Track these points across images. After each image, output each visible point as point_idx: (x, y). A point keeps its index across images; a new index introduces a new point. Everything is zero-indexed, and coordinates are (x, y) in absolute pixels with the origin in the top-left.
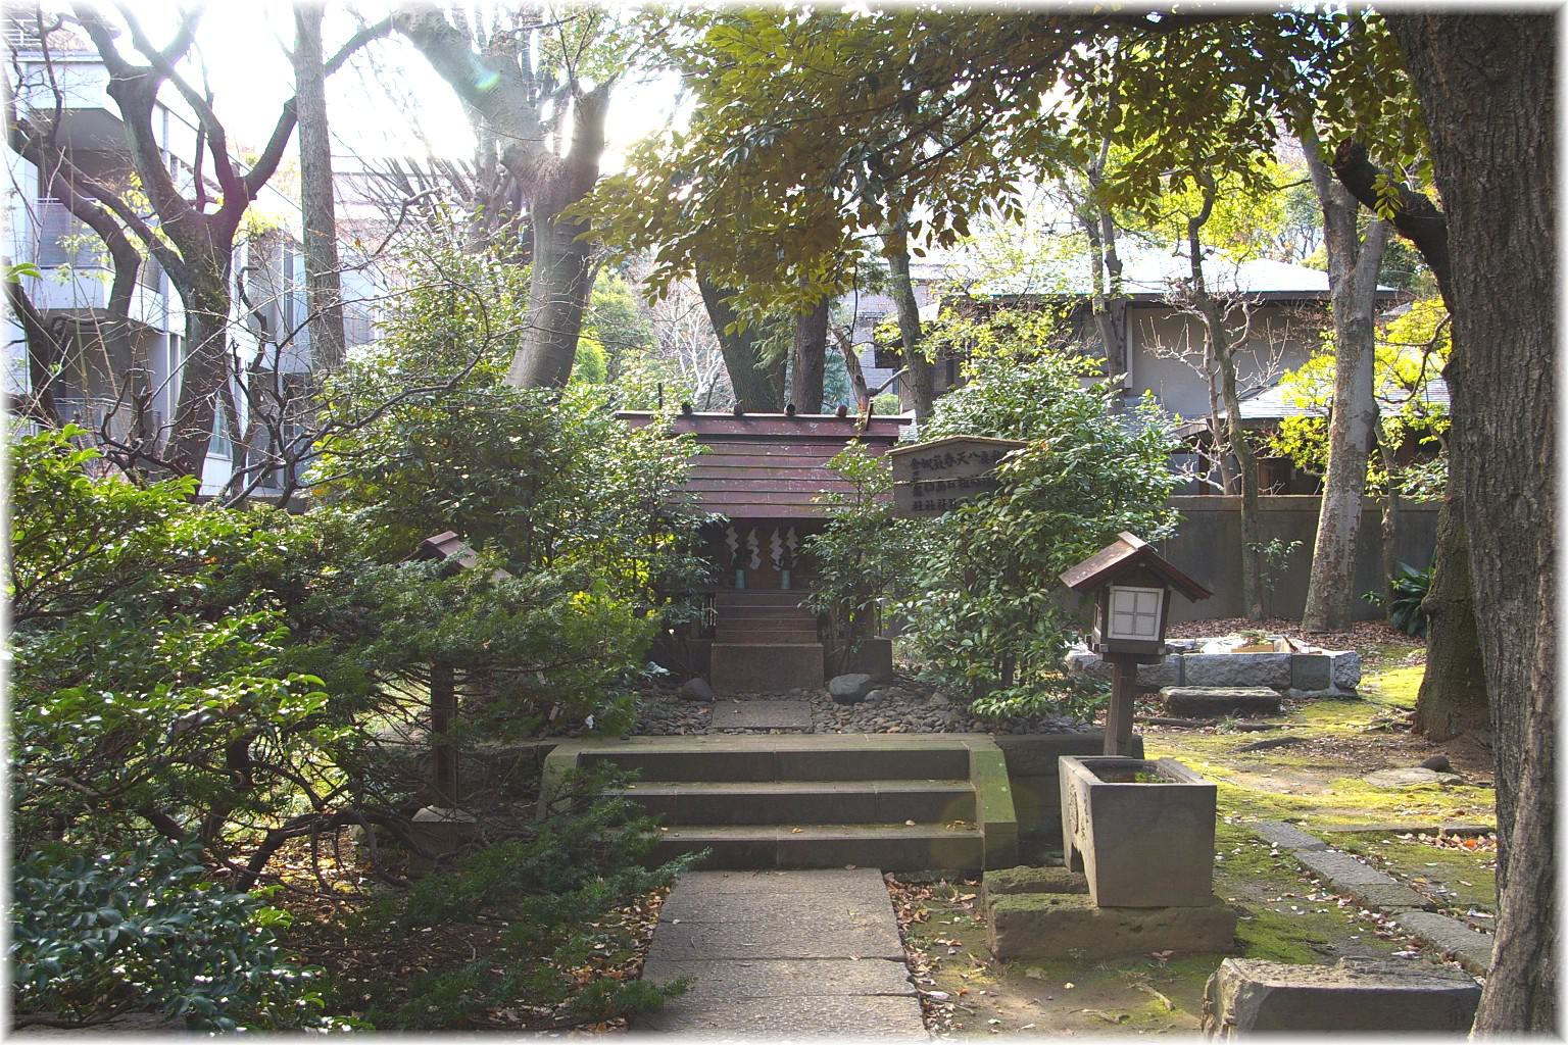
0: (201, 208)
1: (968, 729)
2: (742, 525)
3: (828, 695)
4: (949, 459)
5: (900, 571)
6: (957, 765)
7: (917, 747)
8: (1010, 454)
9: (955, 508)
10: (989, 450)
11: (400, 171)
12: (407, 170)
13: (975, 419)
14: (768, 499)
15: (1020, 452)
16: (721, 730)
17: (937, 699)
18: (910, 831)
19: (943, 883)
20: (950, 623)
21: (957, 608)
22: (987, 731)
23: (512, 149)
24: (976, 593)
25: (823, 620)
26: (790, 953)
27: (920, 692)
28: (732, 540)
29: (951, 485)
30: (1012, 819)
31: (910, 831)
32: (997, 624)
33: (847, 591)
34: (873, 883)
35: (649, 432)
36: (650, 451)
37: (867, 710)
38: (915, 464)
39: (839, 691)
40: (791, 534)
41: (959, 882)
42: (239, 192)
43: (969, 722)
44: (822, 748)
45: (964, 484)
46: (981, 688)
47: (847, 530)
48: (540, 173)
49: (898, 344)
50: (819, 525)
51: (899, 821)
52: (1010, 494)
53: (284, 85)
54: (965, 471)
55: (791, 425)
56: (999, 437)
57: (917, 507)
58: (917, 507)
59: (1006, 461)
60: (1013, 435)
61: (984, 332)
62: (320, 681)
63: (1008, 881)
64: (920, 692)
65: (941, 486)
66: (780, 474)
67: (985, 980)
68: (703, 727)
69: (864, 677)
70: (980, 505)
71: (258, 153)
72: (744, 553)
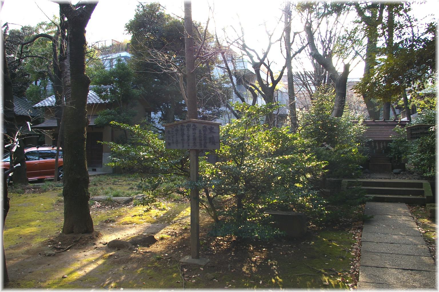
0: (268, 86)
1: (422, 179)
2: (375, 141)
3: (393, 173)
4: (418, 129)
5: (406, 151)
6: (420, 185)
7: (412, 182)
8: (431, 127)
9: (419, 138)
10: (427, 127)
11: (298, 74)
12: (299, 74)
13: (423, 121)
14: (380, 136)
15: (434, 127)
16: (373, 178)
17: (415, 174)
18: (411, 196)
19: (418, 206)
20: (419, 159)
21: (420, 156)
22: (426, 180)
23: (332, 75)
24: (424, 154)
25: (391, 159)
26: (390, 214)
27: (411, 173)
28: (373, 144)
29: (418, 133)
30: (432, 195)
31: (411, 196)
32: (428, 159)
33: (396, 154)
34: (404, 205)
35: (358, 124)
36: (358, 128)
37: (401, 176)
38: (411, 130)
39: (395, 172)
40: (385, 143)
41: (421, 206)
42: (275, 83)
43: (422, 178)
44: (394, 181)
45: (421, 133)
46: (424, 171)
47: (397, 142)
48: (337, 79)
49: (403, 105)
50: (391, 141)
51: (409, 195)
52: (431, 135)
53: (283, 62)
54: (421, 131)
55: (384, 123)
56: (429, 124)
57: (411, 138)
58: (411, 138)
59: (431, 129)
60: (431, 124)
61: (422, 102)
62: (328, 162)
63: (432, 205)
64: (411, 173)
65: (416, 134)
66: (382, 132)
67: (427, 221)
68: (369, 177)
69: (400, 170)
70: (425, 137)
71: (279, 74)
72: (375, 147)
